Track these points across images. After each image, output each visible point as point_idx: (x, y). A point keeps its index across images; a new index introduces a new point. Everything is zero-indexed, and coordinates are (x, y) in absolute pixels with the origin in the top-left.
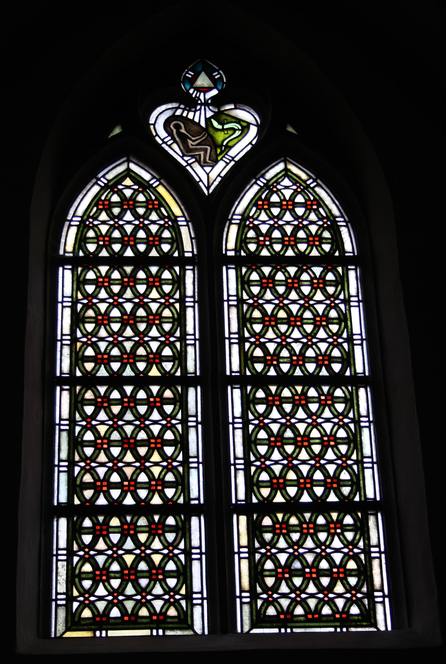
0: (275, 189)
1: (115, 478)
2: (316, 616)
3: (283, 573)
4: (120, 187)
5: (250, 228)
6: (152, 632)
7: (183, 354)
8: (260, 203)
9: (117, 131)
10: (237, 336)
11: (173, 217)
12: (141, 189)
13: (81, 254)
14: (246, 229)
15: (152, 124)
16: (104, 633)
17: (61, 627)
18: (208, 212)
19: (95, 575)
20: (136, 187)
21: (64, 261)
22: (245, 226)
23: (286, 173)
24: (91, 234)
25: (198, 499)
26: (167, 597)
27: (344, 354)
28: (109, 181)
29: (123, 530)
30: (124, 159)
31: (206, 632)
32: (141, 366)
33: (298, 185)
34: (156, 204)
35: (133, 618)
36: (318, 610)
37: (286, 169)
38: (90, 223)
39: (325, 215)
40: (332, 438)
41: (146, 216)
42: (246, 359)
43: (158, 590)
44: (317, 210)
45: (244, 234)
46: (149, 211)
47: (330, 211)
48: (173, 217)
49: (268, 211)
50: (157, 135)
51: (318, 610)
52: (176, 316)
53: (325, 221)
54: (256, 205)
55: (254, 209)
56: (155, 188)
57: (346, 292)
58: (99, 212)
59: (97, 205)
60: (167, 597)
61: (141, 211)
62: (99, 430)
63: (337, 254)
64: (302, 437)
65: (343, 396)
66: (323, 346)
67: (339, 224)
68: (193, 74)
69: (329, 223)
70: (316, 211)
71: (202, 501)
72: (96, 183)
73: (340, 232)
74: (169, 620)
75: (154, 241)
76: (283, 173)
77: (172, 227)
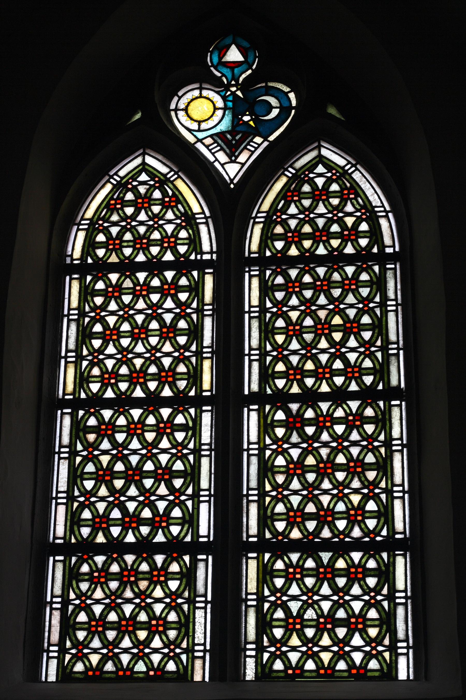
1: (119, 484)
3: (325, 623)
7: (199, 368)
8: (289, 194)
9: (138, 116)
13: (90, 261)
15: (173, 110)
19: (91, 626)
21: (71, 269)
22: (95, 229)
24: (279, 230)
27: (71, 634)
28: (122, 178)
29: (159, 428)
31: (207, 679)
32: (152, 385)
37: (144, 163)
40: (359, 464)
43: (158, 593)
45: (271, 230)
50: (180, 98)
52: (192, 328)
63: (375, 250)
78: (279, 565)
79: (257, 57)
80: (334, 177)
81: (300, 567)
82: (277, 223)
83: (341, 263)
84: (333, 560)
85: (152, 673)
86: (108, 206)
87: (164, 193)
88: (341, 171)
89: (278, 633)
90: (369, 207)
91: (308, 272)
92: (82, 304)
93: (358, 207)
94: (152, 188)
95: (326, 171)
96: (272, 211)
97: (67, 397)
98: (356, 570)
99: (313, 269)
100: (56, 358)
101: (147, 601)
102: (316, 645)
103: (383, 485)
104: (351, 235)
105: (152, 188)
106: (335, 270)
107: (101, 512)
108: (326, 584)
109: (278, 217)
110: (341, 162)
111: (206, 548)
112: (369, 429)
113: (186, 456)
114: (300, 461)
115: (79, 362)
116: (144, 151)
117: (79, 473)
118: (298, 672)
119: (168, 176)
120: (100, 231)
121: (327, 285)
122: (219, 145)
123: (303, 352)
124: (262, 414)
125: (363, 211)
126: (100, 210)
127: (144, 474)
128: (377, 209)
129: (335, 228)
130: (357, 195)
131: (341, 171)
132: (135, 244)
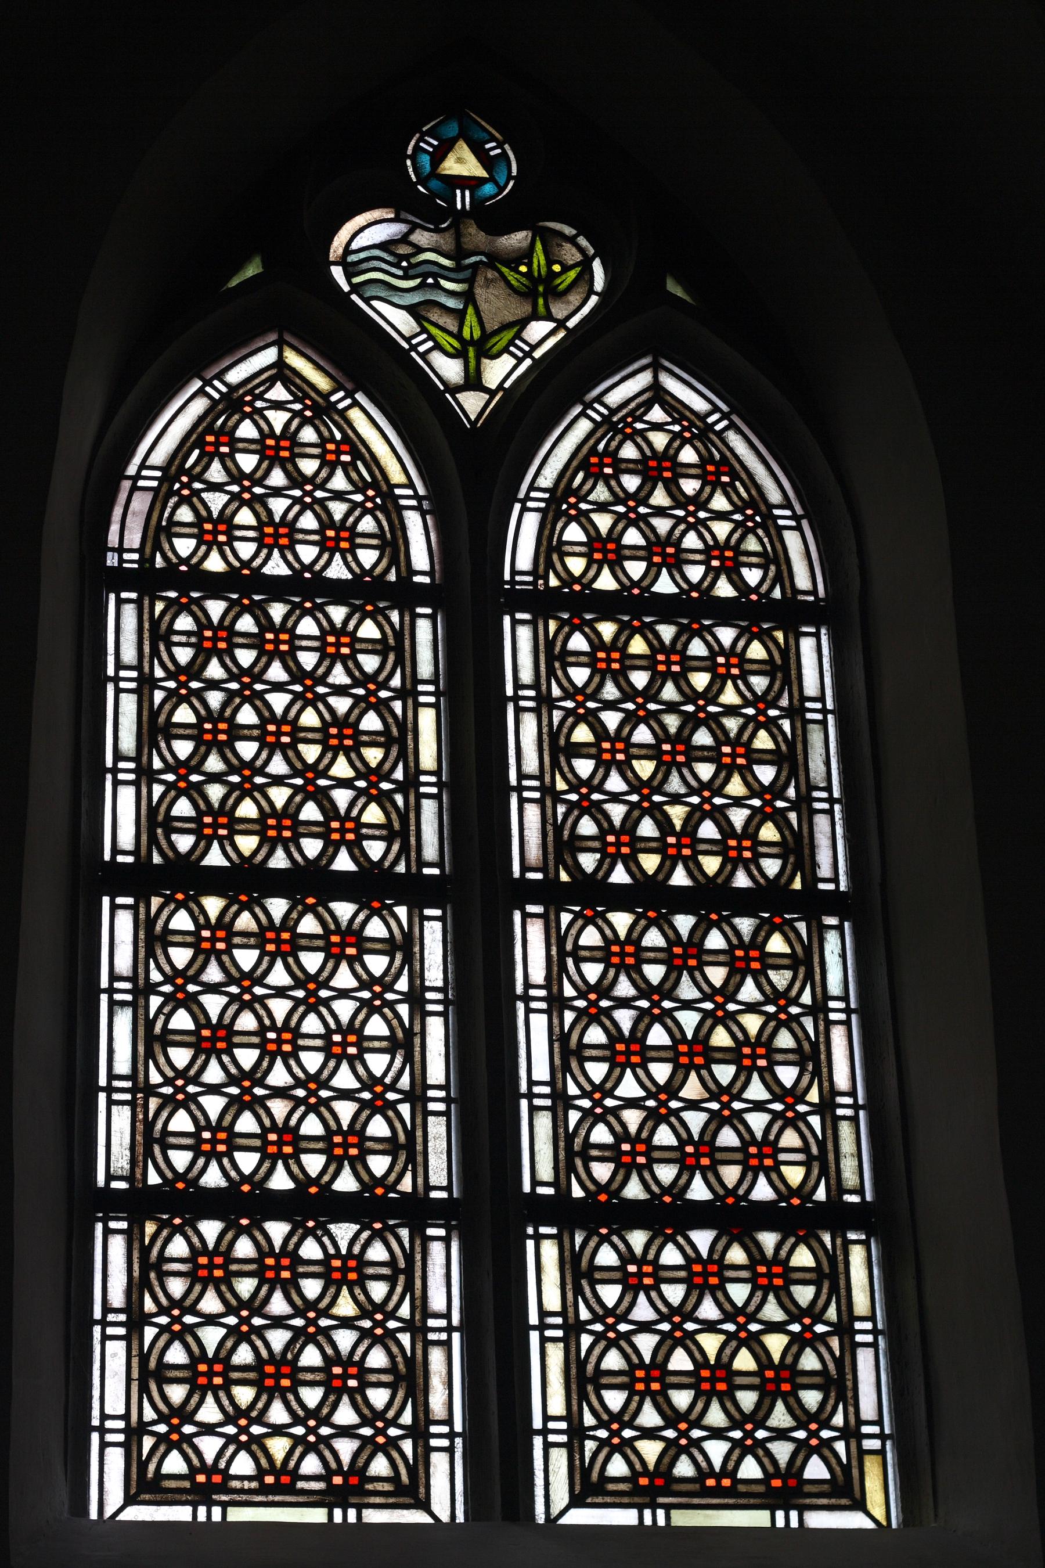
0: (248, 409)
2: (726, 1482)
5: (570, 519)
6: (330, 1516)
8: (210, 439)
9: (252, 270)
11: (385, 488)
16: (202, 1516)
17: (115, 1496)
18: (473, 470)
23: (657, 394)
25: (114, 908)
26: (325, 1431)
28: (613, 412)
30: (273, 337)
31: (460, 1518)
33: (685, 423)
34: (719, 470)
36: (729, 1469)
38: (571, 506)
43: (209, 1412)
44: (731, 484)
47: (759, 488)
48: (385, 488)
49: (613, 483)
51: (729, 1469)
54: (584, 465)
55: (580, 476)
57: (795, 688)
58: (205, 459)
59: (200, 443)
60: (325, 1431)
64: (699, 1166)
65: (789, 951)
68: (436, 143)
71: (106, 901)
72: (583, 414)
79: (409, 157)
83: (320, 597)
86: (584, 465)
91: (249, 609)
98: (211, 1260)
99: (198, 602)
104: (337, 538)
106: (306, 612)
110: (699, 405)
112: (377, 964)
116: (281, 336)
118: (659, 1482)
121: (290, 642)
122: (431, 337)
125: (371, 493)
128: (398, 491)
132: (290, 536)
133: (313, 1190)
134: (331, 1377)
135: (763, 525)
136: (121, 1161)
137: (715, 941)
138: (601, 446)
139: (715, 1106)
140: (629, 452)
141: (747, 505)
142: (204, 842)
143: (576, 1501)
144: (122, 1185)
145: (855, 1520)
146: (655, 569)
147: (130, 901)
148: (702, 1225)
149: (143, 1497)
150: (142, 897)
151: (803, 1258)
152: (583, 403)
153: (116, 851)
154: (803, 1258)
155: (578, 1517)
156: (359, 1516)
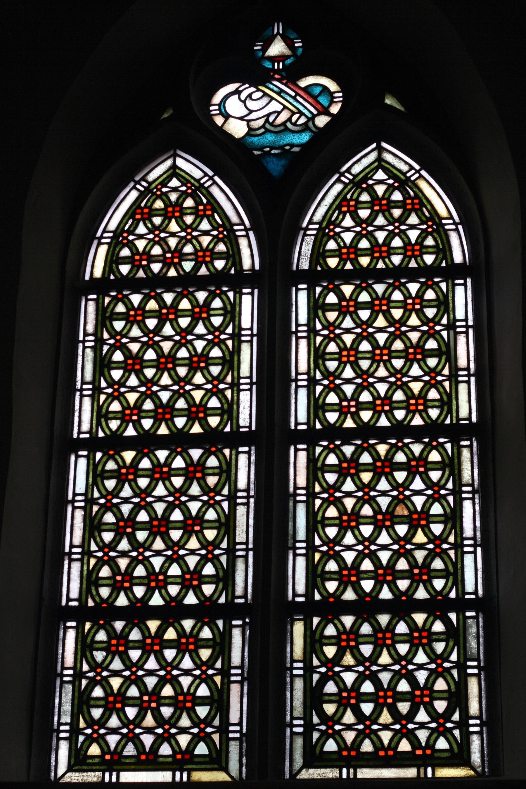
2: (353, 753)
4: (370, 182)
10: (460, 379)
12: (396, 184)
14: (325, 239)
17: (62, 767)
20: (391, 181)
22: (325, 234)
23: (380, 163)
24: (332, 245)
28: (355, 176)
34: (417, 203)
35: (151, 757)
37: (174, 166)
38: (331, 230)
39: (220, 223)
41: (370, 221)
42: (317, 407)
46: (407, 213)
51: (430, 744)
53: (221, 229)
56: (207, 189)
61: (189, 219)
62: (464, 515)
66: (382, 388)
67: (447, 227)
69: (435, 227)
70: (211, 220)
73: (238, 245)
74: (161, 759)
75: (204, 256)
76: (376, 164)
77: (437, 231)
78: (330, 631)
80: (189, 191)
81: (194, 635)
82: (330, 238)
84: (161, 630)
85: (108, 757)
86: (339, 207)
87: (198, 202)
88: (197, 184)
89: (330, 709)
90: (227, 224)
92: (99, 330)
93: (423, 218)
94: (390, 189)
95: (386, 177)
96: (324, 224)
97: (82, 436)
100: (71, 390)
101: (400, 667)
102: (174, 726)
103: (452, 539)
105: (184, 195)
107: (192, 567)
108: (187, 657)
109: (331, 230)
111: (69, 613)
113: (219, 503)
114: (425, 510)
115: (96, 396)
117: (319, 518)
118: (187, 757)
119: (202, 181)
120: (124, 246)
123: (123, 390)
124: (91, 462)
125: (430, 223)
126: (331, 212)
127: (138, 526)
128: (444, 222)
129: (364, 244)
130: (422, 205)
131: (197, 184)
133: (368, 599)
134: (342, 698)
135: (437, 231)
136: (301, 588)
137: (145, 464)
138: (349, 196)
139: (408, 547)
140: (159, 204)
141: (428, 219)
142: (377, 415)
143: (307, 764)
144: (75, 604)
145: (220, 776)
146: (199, 264)
147: (85, 453)
148: (383, 612)
149: (76, 768)
150: (92, 452)
151: (206, 633)
152: (339, 173)
153: (297, 424)
154: (206, 633)
155: (75, 777)
156: (189, 776)
